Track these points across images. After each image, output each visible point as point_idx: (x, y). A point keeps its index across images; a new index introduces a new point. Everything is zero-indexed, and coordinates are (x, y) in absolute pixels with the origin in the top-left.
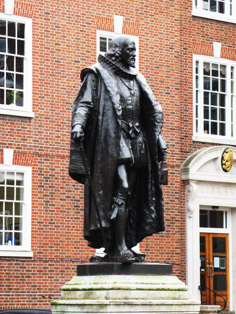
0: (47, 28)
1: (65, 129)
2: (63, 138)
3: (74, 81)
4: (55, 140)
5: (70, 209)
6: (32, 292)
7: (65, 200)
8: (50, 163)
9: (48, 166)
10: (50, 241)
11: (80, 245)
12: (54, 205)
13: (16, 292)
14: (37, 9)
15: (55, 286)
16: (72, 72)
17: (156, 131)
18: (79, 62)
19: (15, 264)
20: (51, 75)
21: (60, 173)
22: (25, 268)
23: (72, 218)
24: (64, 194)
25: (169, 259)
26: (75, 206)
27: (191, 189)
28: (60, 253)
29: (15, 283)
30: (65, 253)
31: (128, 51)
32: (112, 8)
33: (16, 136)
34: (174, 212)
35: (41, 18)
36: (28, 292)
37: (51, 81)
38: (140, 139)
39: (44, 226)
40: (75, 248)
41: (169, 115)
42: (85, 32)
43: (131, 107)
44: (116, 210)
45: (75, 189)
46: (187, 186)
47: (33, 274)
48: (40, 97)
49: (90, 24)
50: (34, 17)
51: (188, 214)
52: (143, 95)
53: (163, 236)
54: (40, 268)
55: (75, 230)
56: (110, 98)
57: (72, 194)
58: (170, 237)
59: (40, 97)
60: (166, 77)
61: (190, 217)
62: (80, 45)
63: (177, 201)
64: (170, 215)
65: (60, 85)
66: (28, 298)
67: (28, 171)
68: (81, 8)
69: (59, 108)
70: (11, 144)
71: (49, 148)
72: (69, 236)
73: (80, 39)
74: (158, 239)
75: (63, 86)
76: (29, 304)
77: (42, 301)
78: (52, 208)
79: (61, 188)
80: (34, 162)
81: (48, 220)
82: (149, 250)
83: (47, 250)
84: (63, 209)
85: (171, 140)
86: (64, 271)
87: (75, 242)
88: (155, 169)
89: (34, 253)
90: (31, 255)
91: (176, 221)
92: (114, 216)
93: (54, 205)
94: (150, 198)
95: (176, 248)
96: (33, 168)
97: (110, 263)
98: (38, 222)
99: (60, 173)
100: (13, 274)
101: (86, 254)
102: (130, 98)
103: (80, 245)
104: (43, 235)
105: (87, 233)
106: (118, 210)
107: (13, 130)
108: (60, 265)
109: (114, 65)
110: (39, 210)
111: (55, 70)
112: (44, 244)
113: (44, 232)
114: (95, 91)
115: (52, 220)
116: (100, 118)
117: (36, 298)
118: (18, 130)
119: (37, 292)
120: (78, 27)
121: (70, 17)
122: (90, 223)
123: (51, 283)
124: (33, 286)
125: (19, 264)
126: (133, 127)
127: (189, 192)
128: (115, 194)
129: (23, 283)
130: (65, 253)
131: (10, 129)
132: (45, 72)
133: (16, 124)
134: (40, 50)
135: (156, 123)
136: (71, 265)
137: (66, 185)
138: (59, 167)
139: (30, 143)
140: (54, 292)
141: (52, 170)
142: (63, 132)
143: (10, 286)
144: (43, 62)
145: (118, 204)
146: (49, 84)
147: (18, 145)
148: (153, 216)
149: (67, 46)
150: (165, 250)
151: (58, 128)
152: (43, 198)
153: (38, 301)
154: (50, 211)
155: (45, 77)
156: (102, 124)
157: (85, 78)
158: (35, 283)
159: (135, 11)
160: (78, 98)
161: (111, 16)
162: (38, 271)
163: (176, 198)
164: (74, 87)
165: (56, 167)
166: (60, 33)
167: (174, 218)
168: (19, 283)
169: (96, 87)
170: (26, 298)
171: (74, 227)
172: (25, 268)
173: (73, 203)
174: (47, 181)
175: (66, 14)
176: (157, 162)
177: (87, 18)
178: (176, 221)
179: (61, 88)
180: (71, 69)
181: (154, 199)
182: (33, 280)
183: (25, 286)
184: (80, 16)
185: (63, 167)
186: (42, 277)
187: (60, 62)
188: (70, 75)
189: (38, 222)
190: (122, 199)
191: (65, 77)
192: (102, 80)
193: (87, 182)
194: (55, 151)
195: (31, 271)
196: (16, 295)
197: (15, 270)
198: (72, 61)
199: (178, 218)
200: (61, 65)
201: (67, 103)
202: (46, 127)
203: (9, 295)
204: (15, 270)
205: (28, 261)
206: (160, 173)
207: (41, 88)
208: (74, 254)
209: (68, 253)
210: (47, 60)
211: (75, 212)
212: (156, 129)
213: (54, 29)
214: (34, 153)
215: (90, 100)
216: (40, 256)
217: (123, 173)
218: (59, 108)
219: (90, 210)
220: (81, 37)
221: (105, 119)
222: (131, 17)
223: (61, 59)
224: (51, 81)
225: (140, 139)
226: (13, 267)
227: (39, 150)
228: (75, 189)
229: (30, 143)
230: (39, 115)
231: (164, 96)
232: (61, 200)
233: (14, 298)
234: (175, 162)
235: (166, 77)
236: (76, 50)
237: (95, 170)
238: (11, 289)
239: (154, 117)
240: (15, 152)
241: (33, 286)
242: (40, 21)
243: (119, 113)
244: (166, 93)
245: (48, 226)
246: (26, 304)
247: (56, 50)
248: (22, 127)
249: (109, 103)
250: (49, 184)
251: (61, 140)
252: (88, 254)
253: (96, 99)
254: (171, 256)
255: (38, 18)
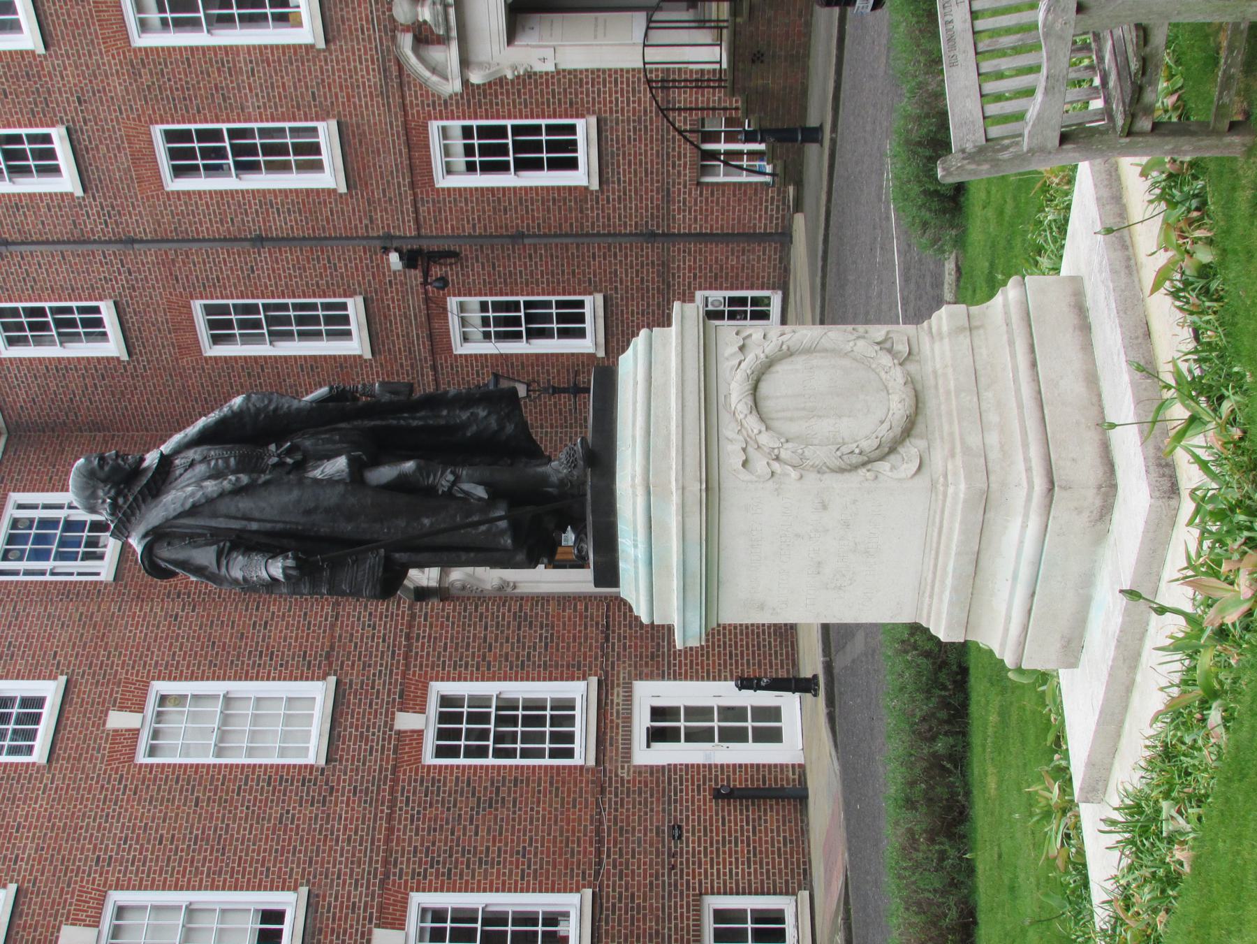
0: (127, 861)
1: (333, 826)
2: (351, 829)
3: (236, 808)
4: (354, 847)
5: (496, 817)
6: (664, 890)
7: (477, 827)
8: (403, 856)
9: (408, 859)
10: (560, 856)
11: (569, 796)
12: (488, 848)
13: (664, 921)
14: (88, 882)
15: (651, 846)
16: (218, 812)
17: (289, 407)
18: (198, 798)
19: (607, 924)
20: (223, 854)
21: (423, 836)
22: (614, 905)
23: (514, 813)
24: (465, 827)
25: (597, 624)
26: (490, 806)
27: (458, 584)
28: (585, 835)
29: (645, 924)
30: (585, 826)
31: (107, 468)
32: (92, 732)
33: (346, 923)
34: (504, 614)
35: (107, 872)
36: (663, 898)
37: (235, 854)
38: (308, 443)
39: (529, 867)
40: (574, 807)
41: (309, 623)
42: (137, 786)
43: (232, 460)
44: (466, 486)
45: (455, 806)
46: (453, 592)
47: (627, 890)
48: (267, 876)
49: (122, 776)
50: (104, 886)
51: (509, 590)
52: (204, 438)
53: (552, 635)
54: (614, 875)
55: (538, 806)
56: (210, 501)
57: (466, 813)
58: (553, 622)
59: (267, 876)
60: (233, 628)
61: (515, 587)
62: (163, 797)
63: (482, 609)
64: (509, 623)
65: (244, 835)
66: (676, 897)
67: (420, 900)
68: (89, 793)
69: (290, 838)
70: (363, 933)
71: (371, 858)
72: (550, 819)
73: (152, 797)
74: (558, 645)
75: (245, 829)
76: (688, 896)
77: (682, 870)
78: (493, 852)
79: (453, 834)
80: (400, 887)
81: (517, 860)
82: (579, 662)
83: (579, 861)
84: (495, 830)
85: (359, 619)
86: (621, 828)
87: (562, 806)
88: (375, 409)
89: (584, 886)
90: (588, 892)
91: (521, 611)
92: (480, 492)
93: (488, 848)
94: (442, 422)
95: (575, 610)
96: (412, 890)
97: (589, 492)
98: (522, 879)
99: (423, 836)
100: (626, 928)
101: (587, 786)
102: (213, 463)
103: (569, 796)
104: (548, 871)
105: (520, 557)
106: (469, 482)
107: (333, 930)
108: (609, 835)
109: (135, 499)
110: (498, 878)
111: (212, 847)
112: (566, 868)
113: (541, 868)
114: (193, 538)
115: (518, 853)
116: (254, 526)
117: (676, 881)
118: (334, 920)
119: (664, 882)
120: (128, 801)
121: (107, 816)
122: (498, 550)
123: (645, 852)
124: (651, 889)
125: (607, 916)
126: (279, 456)
127: (464, 588)
128: (431, 491)
129: (645, 908)
130: (585, 826)
131: (332, 935)
132: (216, 865)
133: (321, 923)
134: (172, 876)
135: (272, 407)
136: (610, 814)
137: (447, 823)
138: (411, 837)
139: (359, 895)
140: (663, 846)
141: (415, 852)
142: (339, 830)
143: (651, 935)
144: (197, 868)
145: (454, 483)
146: (240, 858)
147: (364, 919)
148: (482, 413)
149: (164, 821)
150: (580, 632)
151: (331, 840)
152: (474, 870)
153: (682, 878)
154: (499, 856)
155: (227, 865)
156: (269, 521)
157: (163, 564)
158: (645, 886)
159: (99, 689)
160: (208, 578)
161: (108, 735)
162: (621, 879)
163: (476, 610)
164: (248, 808)
165: (410, 845)
166: (138, 835)
167: (515, 613)
168: (645, 915)
169: (182, 537)
170: (676, 903)
171: (532, 809)
172: (614, 905)
173: (484, 810)
174: (438, 862)
175: (100, 824)
176: (360, 403)
177: (109, 782)
178: (521, 611)
179: (250, 833)
180: (212, 814)
181: (445, 413)
182: (639, 890)
183: (651, 905)
184: (106, 796)
185: (411, 830)
186: (633, 871)
187: (197, 836)
188: (224, 816)
189: (522, 879)
190: (442, 474)
191: (228, 825)
192: (167, 522)
193: (399, 556)
194: (379, 847)
195: (620, 894)
196: (670, 922)
197: (619, 925)
198: (195, 812)
199: (515, 607)
200: (203, 833)
201: (281, 823)
202: (328, 863)
203: (670, 936)
204: (619, 925)
205: (43, 573)
206: (387, 397)
207: (250, 873)
208: (586, 807)
209: (586, 820)
210: (192, 862)
211: (503, 807)
212: (286, 406)
213: (130, 846)
214: (381, 888)
215: (215, 547)
216: (590, 875)
217: (385, 473)
218: (290, 838)
219: (467, 549)
220: (147, 793)
221: (257, 515)
222: (111, 696)
223: (191, 833)
224: (235, 854)
225: (308, 443)
226: (613, 927)
227: (375, 877)
228: (455, 806)
229: (359, 895)
230: (303, 878)
231: (270, 631)
232: (476, 834)
233: (676, 925)
234: (403, 612)
235: (233, 628)
236: (173, 804)
237: (375, 536)
238: (657, 931)
239: (258, 411)
240: (378, 926)
241: (651, 889)
242: (113, 875)
243: (245, 479)
244: (265, 628)
245: (530, 859)
246: (688, 903)
247: (172, 843)
248: (329, 911)
249: (223, 506)
250: (445, 858)
251: (356, 834)
252: (587, 782)
253: (215, 536)
254: (592, 620)
255: (106, 879)
